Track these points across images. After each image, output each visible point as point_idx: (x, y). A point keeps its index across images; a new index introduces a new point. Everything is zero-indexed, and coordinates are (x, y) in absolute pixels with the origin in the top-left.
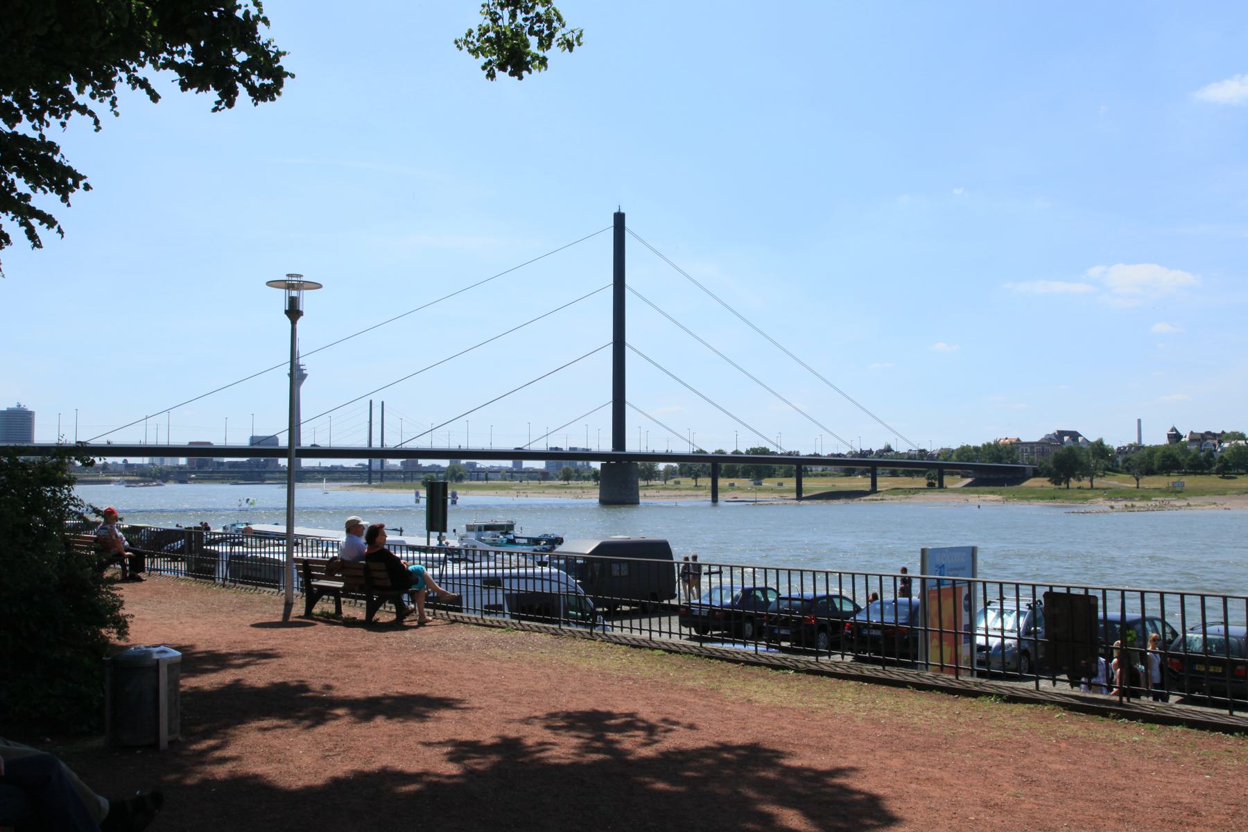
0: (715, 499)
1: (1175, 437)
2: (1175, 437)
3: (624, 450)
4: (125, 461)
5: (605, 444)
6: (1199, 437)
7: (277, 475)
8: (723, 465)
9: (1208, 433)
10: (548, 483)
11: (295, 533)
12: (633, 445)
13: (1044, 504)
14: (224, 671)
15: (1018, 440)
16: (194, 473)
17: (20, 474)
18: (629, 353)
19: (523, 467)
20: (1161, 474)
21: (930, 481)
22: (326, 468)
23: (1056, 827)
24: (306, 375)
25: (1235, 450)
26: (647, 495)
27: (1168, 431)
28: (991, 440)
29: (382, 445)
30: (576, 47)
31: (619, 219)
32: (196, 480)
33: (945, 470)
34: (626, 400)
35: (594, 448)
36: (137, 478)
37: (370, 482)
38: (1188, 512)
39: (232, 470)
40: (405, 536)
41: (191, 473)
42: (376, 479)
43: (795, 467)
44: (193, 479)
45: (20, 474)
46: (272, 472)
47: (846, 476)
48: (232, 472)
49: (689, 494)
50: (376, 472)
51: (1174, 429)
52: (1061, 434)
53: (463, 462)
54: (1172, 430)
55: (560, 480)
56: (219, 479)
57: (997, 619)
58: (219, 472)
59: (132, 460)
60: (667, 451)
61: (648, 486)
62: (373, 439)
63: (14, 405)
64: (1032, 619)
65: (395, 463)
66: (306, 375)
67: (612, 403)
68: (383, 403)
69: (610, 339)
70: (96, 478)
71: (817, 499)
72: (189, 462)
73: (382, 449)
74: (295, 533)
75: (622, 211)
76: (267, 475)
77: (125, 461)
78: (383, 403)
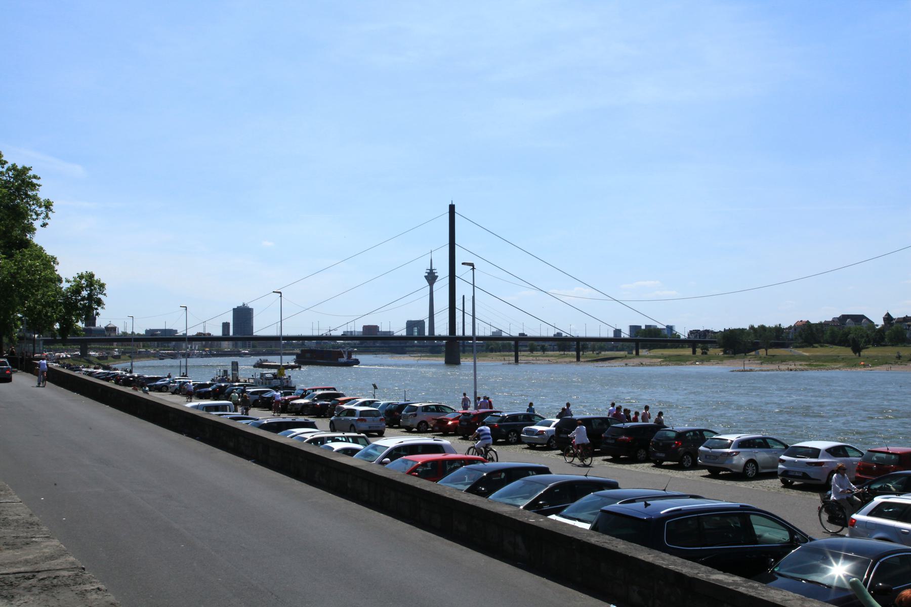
3: (455, 335)
6: (902, 320)
7: (415, 349)
13: (723, 367)
15: (907, 316)
18: (457, 281)
20: (672, 348)
24: (437, 276)
25: (899, 329)
26: (644, 363)
27: (884, 315)
31: (452, 208)
38: (625, 369)
39: (383, 345)
44: (356, 351)
48: (383, 347)
49: (147, 365)
51: (888, 314)
52: (844, 318)
54: (886, 315)
55: (556, 351)
56: (374, 352)
58: (375, 347)
62: (465, 324)
63: (240, 304)
64: (161, 387)
66: (437, 276)
67: (448, 309)
69: (448, 274)
75: (453, 204)
76: (407, 349)
78: (464, 296)
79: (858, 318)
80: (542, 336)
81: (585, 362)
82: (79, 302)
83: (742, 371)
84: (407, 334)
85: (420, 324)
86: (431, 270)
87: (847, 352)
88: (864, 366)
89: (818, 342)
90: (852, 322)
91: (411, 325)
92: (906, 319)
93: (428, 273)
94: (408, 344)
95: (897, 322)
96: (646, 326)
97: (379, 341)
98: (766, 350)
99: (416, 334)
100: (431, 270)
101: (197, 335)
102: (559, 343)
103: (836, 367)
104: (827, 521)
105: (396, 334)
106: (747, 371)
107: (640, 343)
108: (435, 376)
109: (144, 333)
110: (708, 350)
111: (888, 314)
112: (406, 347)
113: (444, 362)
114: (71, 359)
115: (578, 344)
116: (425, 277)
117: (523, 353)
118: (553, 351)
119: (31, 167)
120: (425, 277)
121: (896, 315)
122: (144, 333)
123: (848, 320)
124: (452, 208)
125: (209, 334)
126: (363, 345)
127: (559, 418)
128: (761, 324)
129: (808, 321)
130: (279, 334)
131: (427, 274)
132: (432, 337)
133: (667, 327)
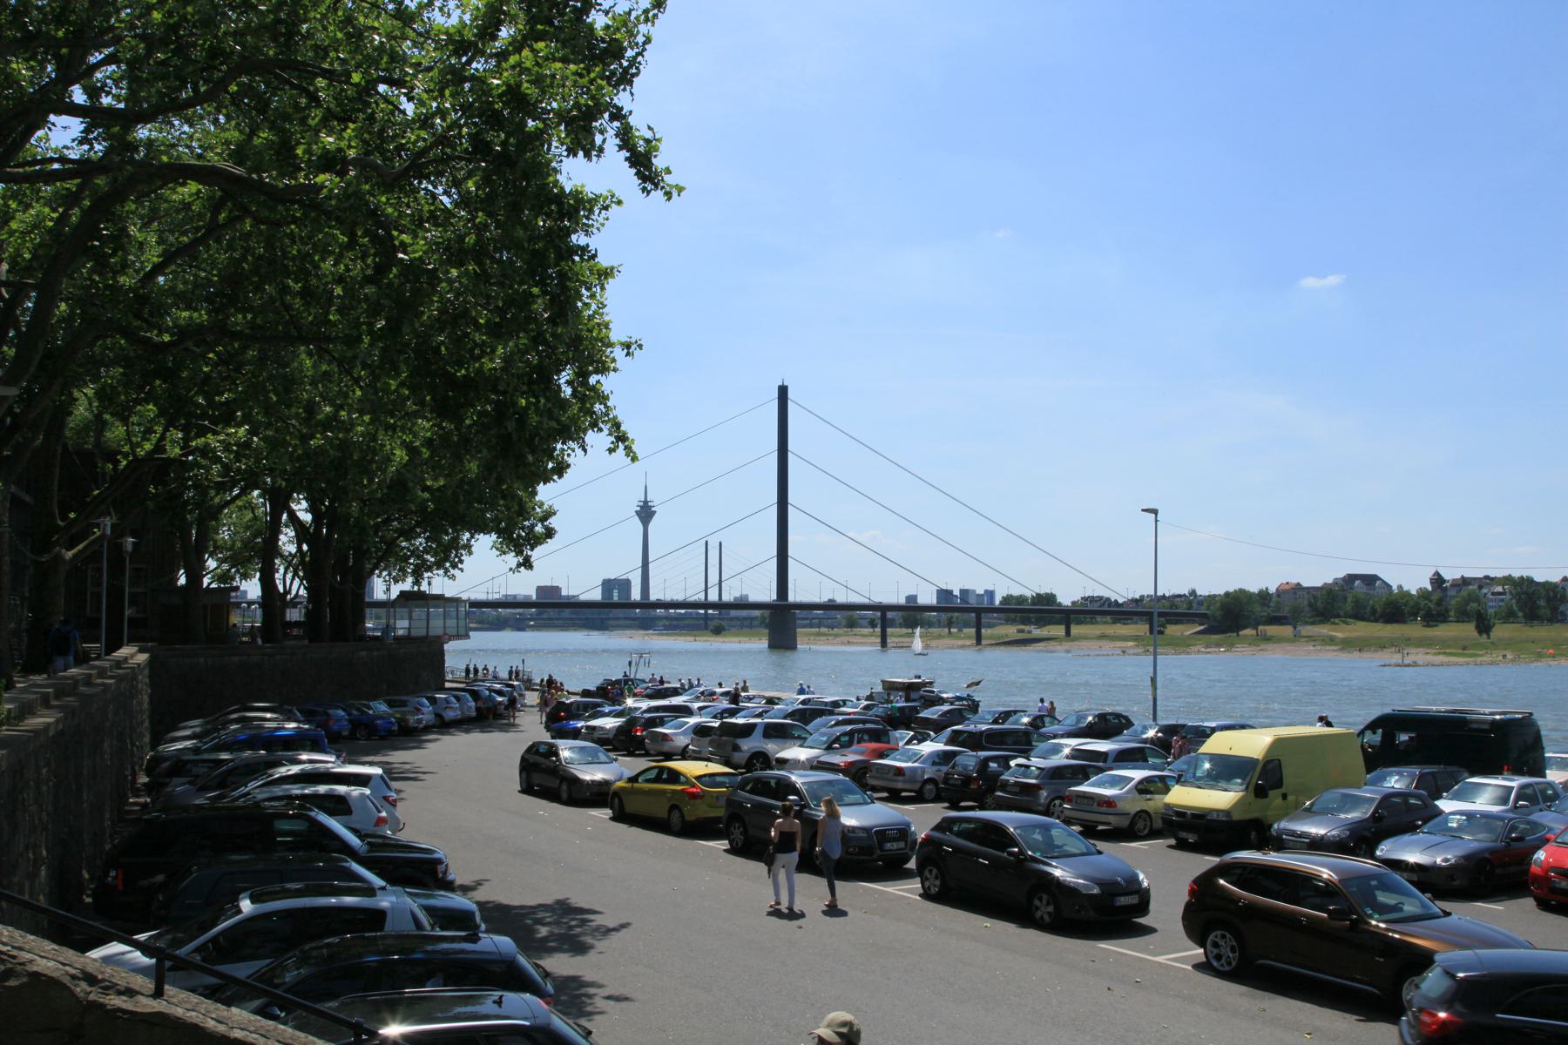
0: (884, 643)
1: (1438, 580)
2: (1438, 580)
3: (787, 600)
5: (768, 594)
8: (1072, 616)
9: (1487, 577)
12: (793, 597)
17: (220, 74)
24: (655, 512)
28: (1231, 588)
30: (637, 352)
31: (783, 392)
32: (533, 628)
35: (755, 597)
39: (573, 616)
41: (531, 620)
43: (879, 614)
44: (532, 626)
45: (220, 74)
48: (572, 619)
51: (1437, 574)
52: (1351, 578)
53: (672, 611)
54: (1434, 575)
57: (1490, 830)
58: (560, 619)
66: (655, 512)
68: (720, 543)
76: (610, 622)
79: (1370, 580)
81: (991, 645)
82: (520, 528)
83: (1399, 666)
85: (625, 585)
86: (646, 502)
87: (1469, 630)
88: (1553, 656)
89: (1338, 616)
90: (1362, 585)
91: (608, 585)
92: (1565, 579)
94: (611, 616)
95: (1452, 585)
96: (961, 590)
97: (568, 610)
99: (616, 598)
100: (646, 502)
102: (904, 613)
105: (583, 598)
106: (1409, 665)
109: (1070, 604)
110: (1165, 627)
111: (1437, 574)
112: (609, 619)
113: (766, 645)
115: (883, 617)
117: (897, 630)
118: (811, 627)
119: (680, 190)
121: (1449, 575)
122: (1070, 604)
123: (1357, 583)
124: (783, 392)
126: (545, 616)
128: (1044, 590)
129: (1299, 584)
130: (702, 597)
131: (639, 509)
132: (646, 605)
133: (986, 591)
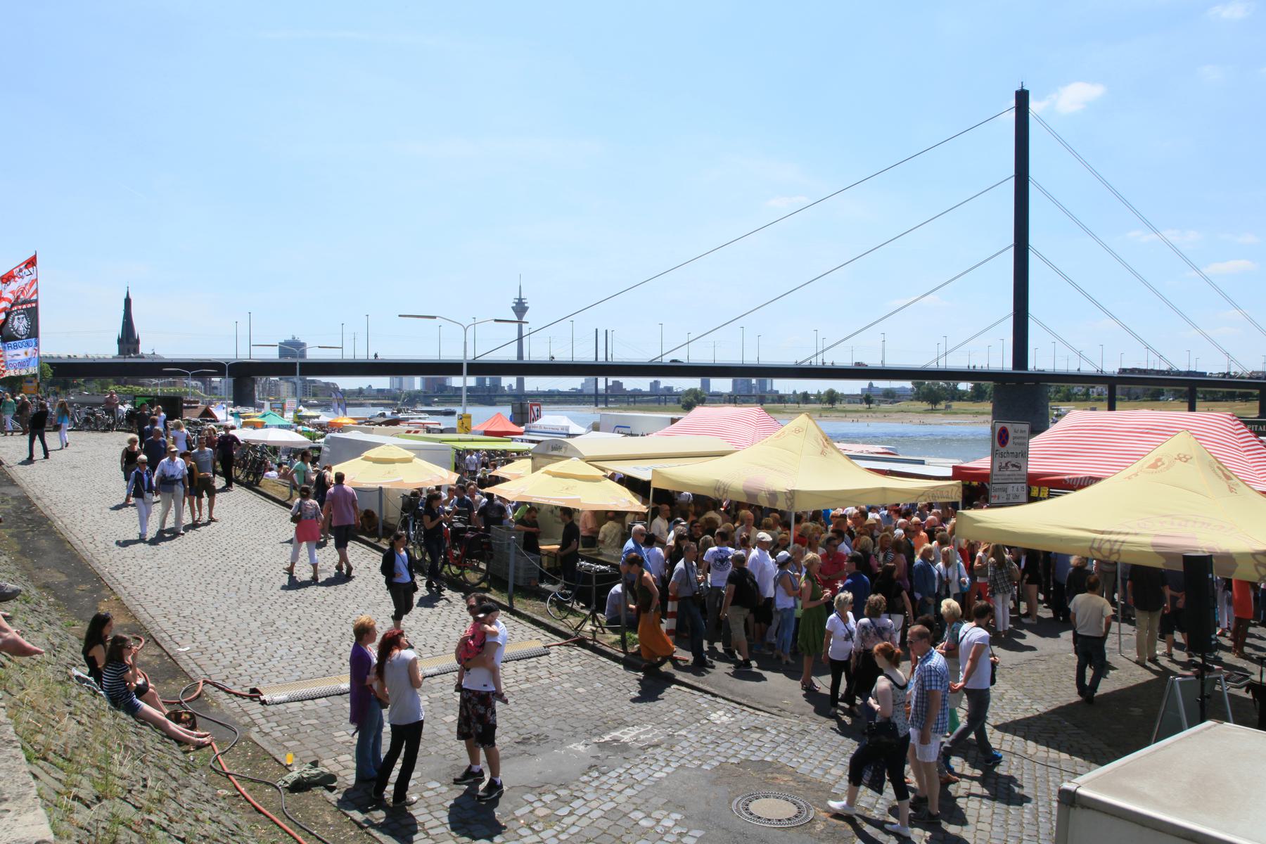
3: (1026, 367)
4: (871, 385)
10: (896, 406)
11: (1258, 402)
14: (95, 564)
16: (437, 397)
19: (711, 391)
21: (967, 483)
22: (545, 392)
23: (247, 822)
24: (527, 308)
29: (520, 355)
33: (1198, 389)
34: (1031, 242)
36: (390, 402)
37: (597, 405)
40: (1199, 411)
42: (602, 402)
44: (436, 402)
46: (501, 396)
47: (1152, 400)
50: (602, 395)
59: (665, 382)
60: (1079, 370)
61: (932, 409)
65: (964, 386)
66: (527, 308)
70: (356, 402)
71: (131, 541)
72: (425, 384)
73: (606, 363)
74: (1258, 402)
75: (1025, 88)
76: (497, 399)
77: (871, 385)
80: (1037, 368)
84: (709, 381)
86: (520, 299)
93: (516, 303)
98: (128, 339)
100: (520, 299)
101: (632, 391)
103: (945, 421)
104: (392, 617)
107: (1118, 387)
108: (1041, 597)
114: (419, 801)
116: (513, 308)
120: (513, 308)
125: (640, 390)
127: (902, 738)
131: (514, 305)
